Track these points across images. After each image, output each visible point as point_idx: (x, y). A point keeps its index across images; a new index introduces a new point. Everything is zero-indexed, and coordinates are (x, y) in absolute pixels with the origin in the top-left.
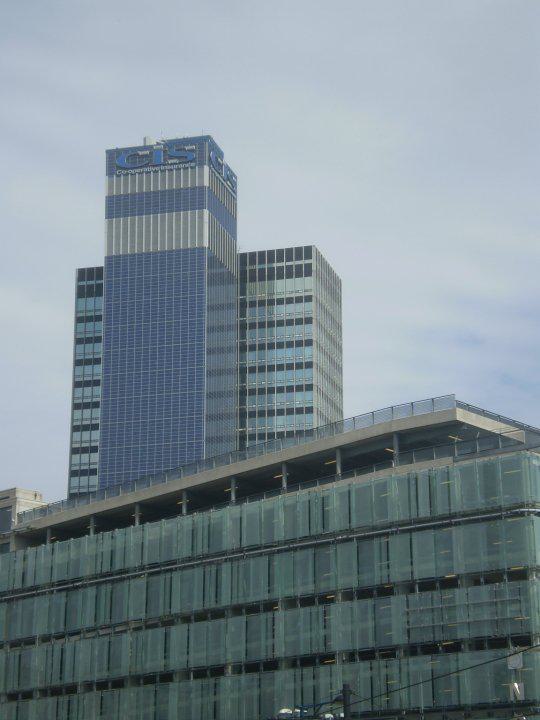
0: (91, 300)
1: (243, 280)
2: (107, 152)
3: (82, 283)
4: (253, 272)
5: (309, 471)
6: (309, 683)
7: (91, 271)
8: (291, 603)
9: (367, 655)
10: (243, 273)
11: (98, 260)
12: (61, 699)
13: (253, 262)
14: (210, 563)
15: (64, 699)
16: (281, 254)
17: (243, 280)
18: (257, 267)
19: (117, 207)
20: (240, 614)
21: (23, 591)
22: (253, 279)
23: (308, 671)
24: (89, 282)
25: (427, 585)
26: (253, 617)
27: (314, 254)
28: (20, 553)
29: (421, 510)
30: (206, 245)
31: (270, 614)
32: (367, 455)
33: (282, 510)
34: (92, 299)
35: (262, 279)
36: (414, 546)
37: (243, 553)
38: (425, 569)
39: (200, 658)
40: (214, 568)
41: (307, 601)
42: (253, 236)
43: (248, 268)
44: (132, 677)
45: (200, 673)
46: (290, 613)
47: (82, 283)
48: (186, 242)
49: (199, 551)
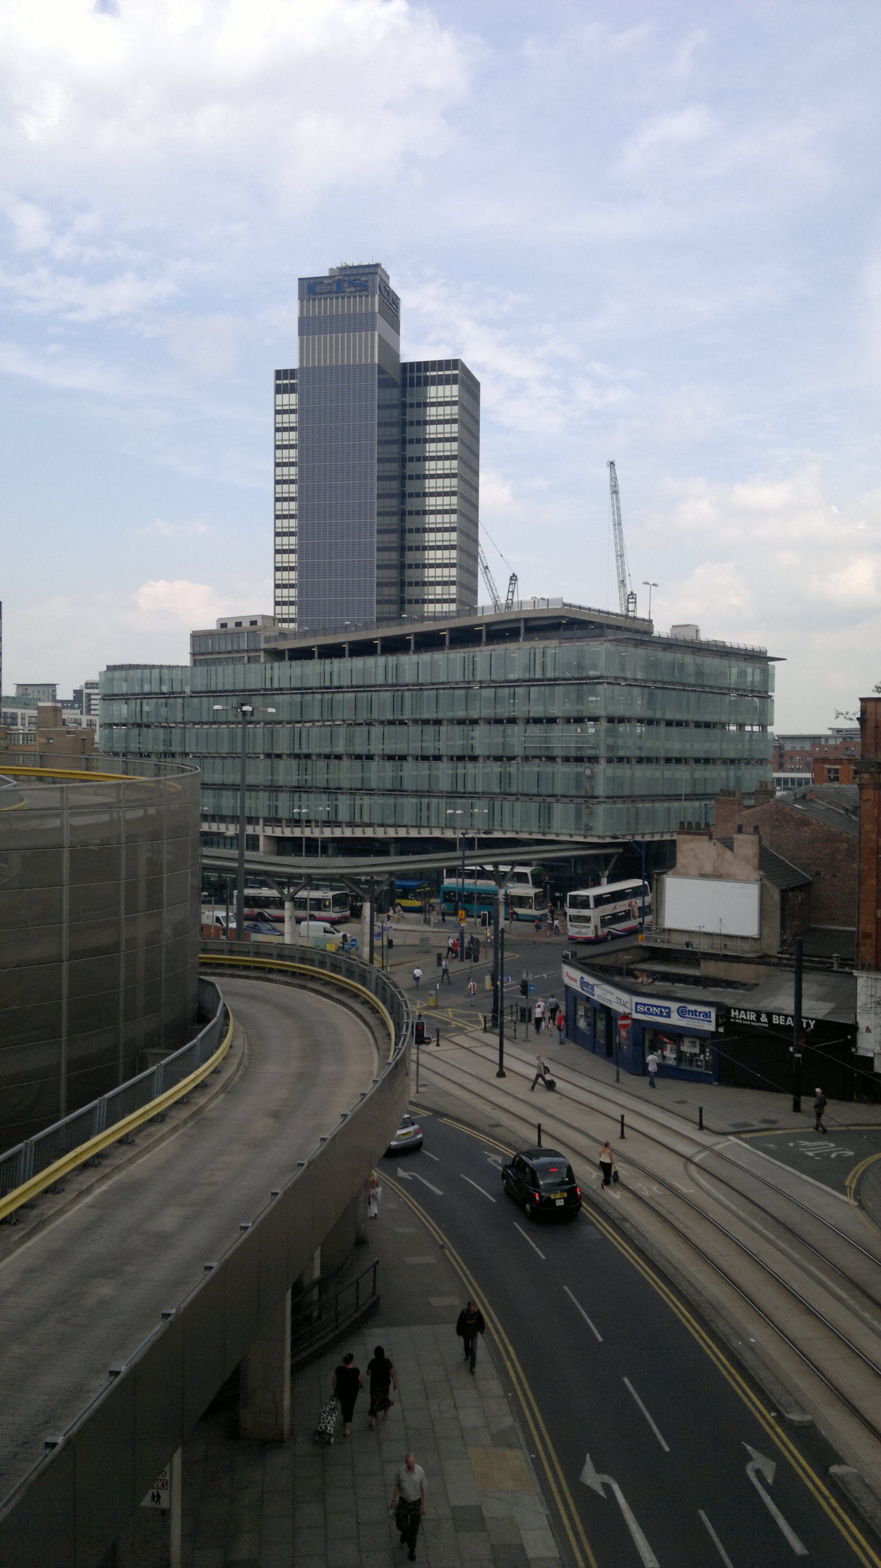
0: (286, 396)
1: (404, 385)
2: (299, 279)
3: (279, 382)
4: (412, 379)
5: (465, 637)
6: (461, 771)
7: (285, 371)
8: (451, 721)
9: (498, 759)
10: (404, 379)
11: (292, 362)
12: (301, 762)
13: (412, 371)
14: (398, 690)
15: (303, 762)
16: (433, 363)
17: (404, 385)
18: (415, 375)
19: (306, 326)
20: (418, 724)
21: (271, 690)
22: (412, 385)
23: (460, 765)
24: (284, 381)
25: (537, 721)
26: (426, 728)
27: (459, 367)
28: (269, 665)
29: (537, 673)
30: (376, 361)
31: (437, 728)
32: (506, 630)
33: (447, 663)
34: (287, 395)
35: (419, 385)
36: (566, 1084)
37: (419, 687)
38: (537, 711)
39: (390, 748)
40: (400, 693)
41: (461, 722)
42: (411, 352)
43: (408, 375)
44: (347, 754)
45: (391, 758)
46: (450, 727)
47: (279, 382)
48: (355, 336)
49: (390, 681)
